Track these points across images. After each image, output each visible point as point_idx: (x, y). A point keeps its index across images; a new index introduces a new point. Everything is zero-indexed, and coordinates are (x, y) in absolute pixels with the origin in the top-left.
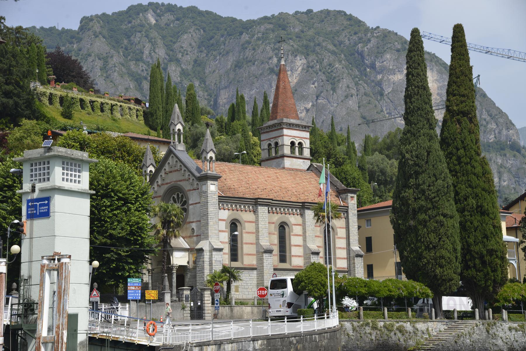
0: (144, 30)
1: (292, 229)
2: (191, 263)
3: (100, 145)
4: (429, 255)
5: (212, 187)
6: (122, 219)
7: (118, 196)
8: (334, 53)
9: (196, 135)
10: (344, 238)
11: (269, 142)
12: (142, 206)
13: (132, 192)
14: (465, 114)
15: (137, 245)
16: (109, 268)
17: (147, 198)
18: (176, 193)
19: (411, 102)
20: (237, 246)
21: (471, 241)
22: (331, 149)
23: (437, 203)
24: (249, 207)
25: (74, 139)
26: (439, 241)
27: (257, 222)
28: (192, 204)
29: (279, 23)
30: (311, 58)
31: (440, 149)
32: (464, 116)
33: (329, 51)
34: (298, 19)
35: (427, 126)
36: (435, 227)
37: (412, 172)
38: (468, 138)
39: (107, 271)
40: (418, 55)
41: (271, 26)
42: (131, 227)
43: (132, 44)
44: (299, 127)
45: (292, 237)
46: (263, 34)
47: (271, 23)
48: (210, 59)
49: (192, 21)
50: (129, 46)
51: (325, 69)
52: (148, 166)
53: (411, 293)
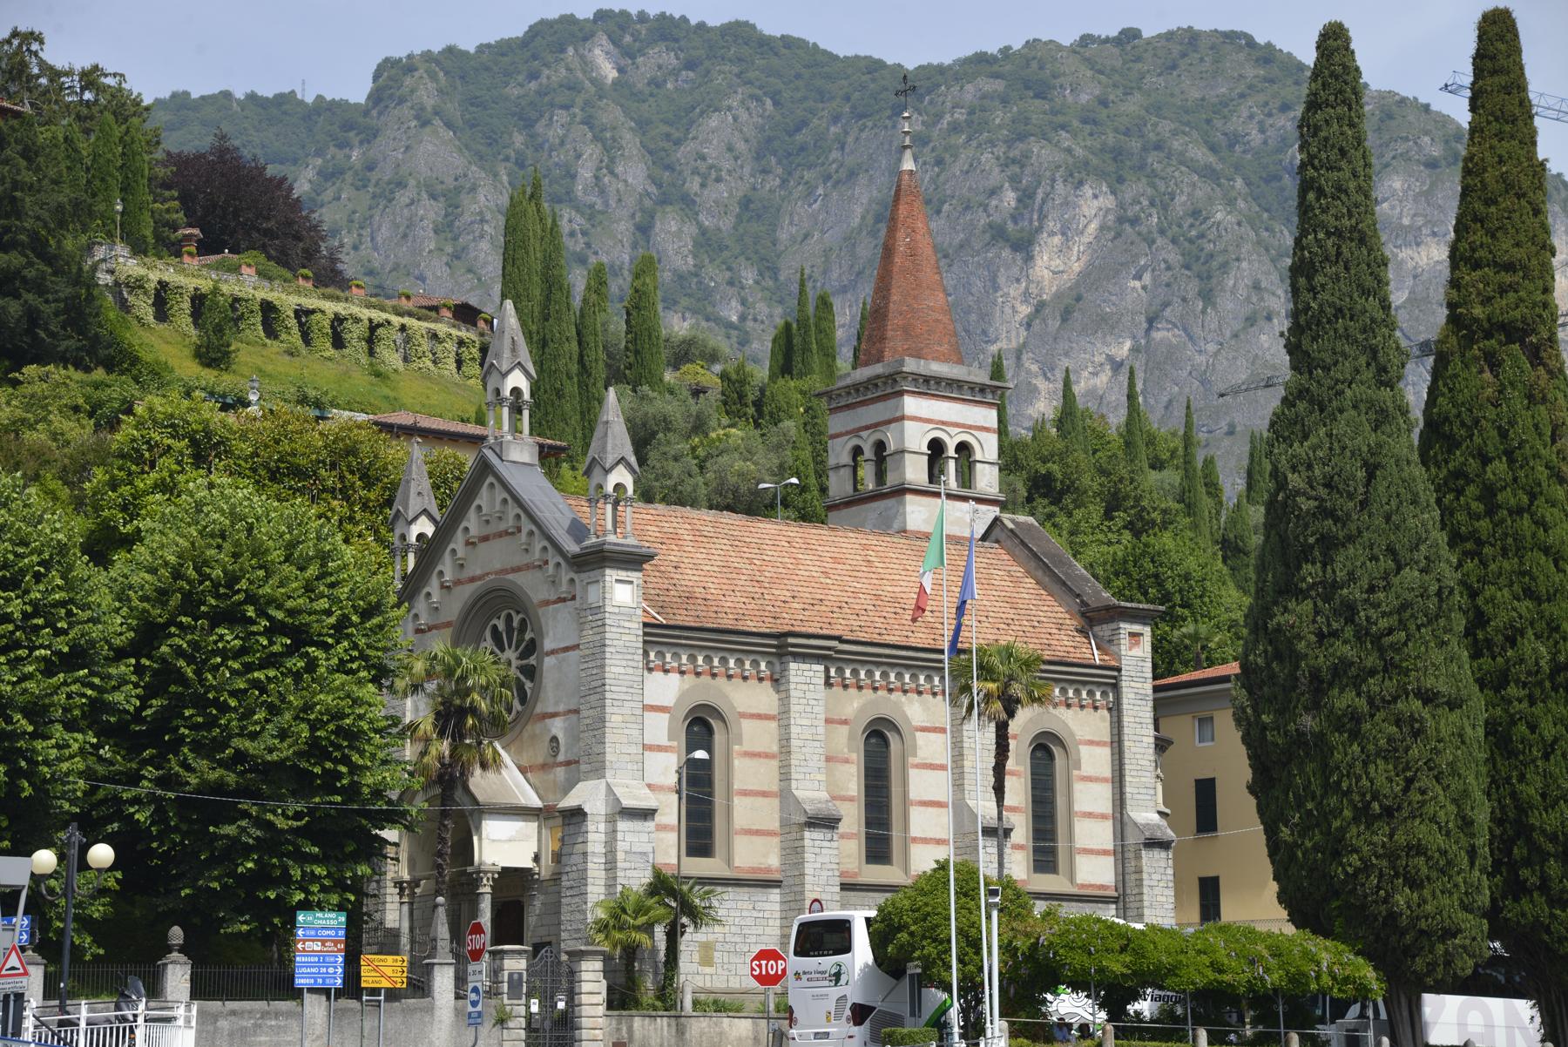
0: (579, 101)
2: (547, 860)
3: (267, 446)
4: (1366, 841)
5: (621, 593)
6: (283, 701)
7: (270, 618)
8: (1208, 173)
9: (644, 425)
10: (1104, 780)
11: (855, 442)
12: (363, 657)
13: (323, 604)
14: (1513, 332)
15: (337, 792)
17: (381, 627)
18: (502, 616)
19: (1312, 289)
20: (711, 803)
21: (1530, 791)
23: (1398, 651)
24: (755, 663)
25: (173, 426)
26: (1406, 790)
27: (783, 717)
28: (553, 652)
29: (1025, 74)
30: (1131, 189)
31: (1415, 457)
32: (1510, 341)
33: (1192, 167)
35: (1368, 375)
36: (1390, 740)
37: (1311, 540)
38: (1525, 419)
39: (225, 887)
41: (999, 86)
42: (313, 729)
43: (538, 148)
45: (912, 773)
46: (971, 112)
47: (996, 76)
48: (796, 195)
49: (736, 70)
50: (529, 152)
51: (1180, 226)
52: (411, 516)
53: (1298, 979)
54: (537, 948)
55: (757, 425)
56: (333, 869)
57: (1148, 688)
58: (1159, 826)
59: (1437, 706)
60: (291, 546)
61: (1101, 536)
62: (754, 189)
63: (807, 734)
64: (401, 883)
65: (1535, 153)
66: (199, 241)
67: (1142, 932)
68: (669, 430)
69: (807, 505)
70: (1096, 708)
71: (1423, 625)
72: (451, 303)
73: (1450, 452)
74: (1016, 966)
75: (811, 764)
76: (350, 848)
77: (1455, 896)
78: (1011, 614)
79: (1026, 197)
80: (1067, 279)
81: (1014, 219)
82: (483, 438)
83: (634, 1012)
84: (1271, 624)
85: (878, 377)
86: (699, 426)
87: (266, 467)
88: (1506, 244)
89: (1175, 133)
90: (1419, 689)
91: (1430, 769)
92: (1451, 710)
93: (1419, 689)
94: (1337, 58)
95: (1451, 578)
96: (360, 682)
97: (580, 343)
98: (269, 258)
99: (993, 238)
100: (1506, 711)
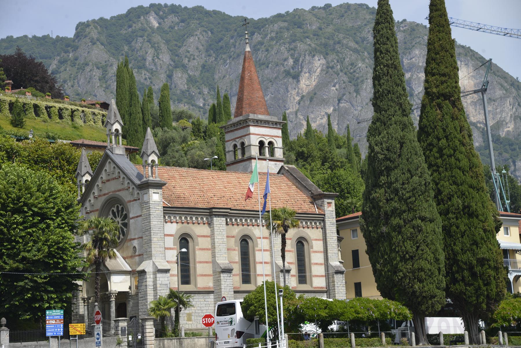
0: (146, 34)
1: (257, 244)
2: (133, 288)
3: (33, 153)
4: (405, 268)
5: (155, 197)
6: (39, 239)
7: (33, 211)
8: (356, 51)
10: (321, 252)
11: (234, 143)
12: (66, 222)
13: (51, 205)
14: (446, 97)
15: (59, 269)
16: (23, 299)
17: (72, 212)
18: (115, 207)
19: (380, 85)
20: (189, 266)
21: (457, 248)
22: (327, 152)
24: (202, 218)
26: (417, 250)
27: (212, 236)
28: (133, 218)
29: (294, 20)
31: (416, 139)
32: (445, 99)
33: (350, 49)
34: (315, 16)
35: (399, 112)
37: (383, 168)
38: (451, 125)
39: (20, 303)
40: (386, 27)
41: (285, 24)
42: (49, 248)
43: (133, 51)
44: (268, 123)
46: (277, 33)
47: (285, 21)
48: (220, 63)
49: (198, 22)
50: (130, 52)
51: (347, 69)
52: (83, 174)
53: (384, 315)
54: (131, 318)
55: (205, 139)
56: (59, 295)
57: (334, 220)
58: (340, 267)
59: (426, 222)
60: (40, 186)
61: (321, 171)
62: (206, 62)
63: (221, 241)
64: (84, 299)
65: (451, 37)
66: (12, 85)
67: (332, 302)
68: (174, 142)
69: (219, 165)
70: (317, 228)
71: (420, 195)
72: (99, 102)
73: (427, 137)
74: (290, 316)
75: (222, 251)
76: (64, 288)
77: (434, 284)
78: (288, 198)
79: (296, 61)
80: (311, 88)
81: (293, 68)
82: (105, 147)
83: (165, 338)
84: (371, 197)
85: (241, 121)
86: (184, 140)
87: (33, 160)
88: (443, 67)
89: (344, 38)
90: (420, 216)
91: (425, 243)
92: (431, 223)
93: (420, 216)
94: (384, 7)
95: (429, 179)
96: (65, 231)
97: (143, 114)
98: (37, 89)
99: (286, 75)
100: (449, 222)
